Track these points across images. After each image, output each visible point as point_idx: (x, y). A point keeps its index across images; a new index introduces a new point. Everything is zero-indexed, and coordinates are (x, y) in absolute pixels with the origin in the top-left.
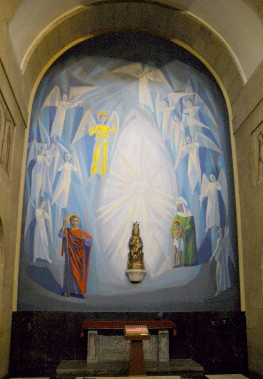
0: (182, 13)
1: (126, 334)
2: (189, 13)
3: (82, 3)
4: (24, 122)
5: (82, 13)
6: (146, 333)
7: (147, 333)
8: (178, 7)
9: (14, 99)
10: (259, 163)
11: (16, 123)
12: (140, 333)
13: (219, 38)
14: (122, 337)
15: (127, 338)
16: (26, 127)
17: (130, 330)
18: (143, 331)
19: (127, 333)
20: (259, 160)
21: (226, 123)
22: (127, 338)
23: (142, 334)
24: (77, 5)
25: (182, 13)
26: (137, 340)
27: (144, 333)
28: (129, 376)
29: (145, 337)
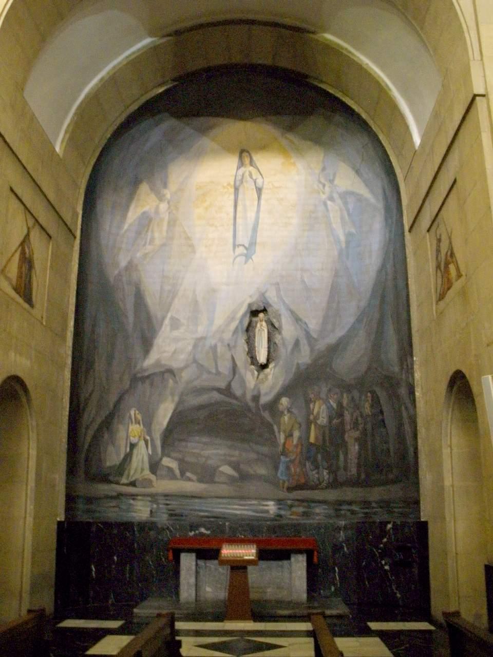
0: (316, 37)
1: (221, 556)
2: (329, 36)
3: (151, 34)
4: (70, 231)
5: (153, 50)
6: (253, 556)
7: (255, 555)
8: (304, 26)
9: (477, 36)
10: (437, 271)
11: (51, 233)
12: (243, 556)
13: (77, 109)
14: (216, 562)
15: (223, 563)
16: (75, 237)
17: (228, 551)
18: (248, 552)
19: (223, 555)
20: (437, 268)
21: (355, 594)
22: (223, 563)
23: (246, 556)
24: (140, 39)
25: (316, 37)
26: (239, 567)
27: (250, 556)
28: (225, 621)
29: (250, 562)
